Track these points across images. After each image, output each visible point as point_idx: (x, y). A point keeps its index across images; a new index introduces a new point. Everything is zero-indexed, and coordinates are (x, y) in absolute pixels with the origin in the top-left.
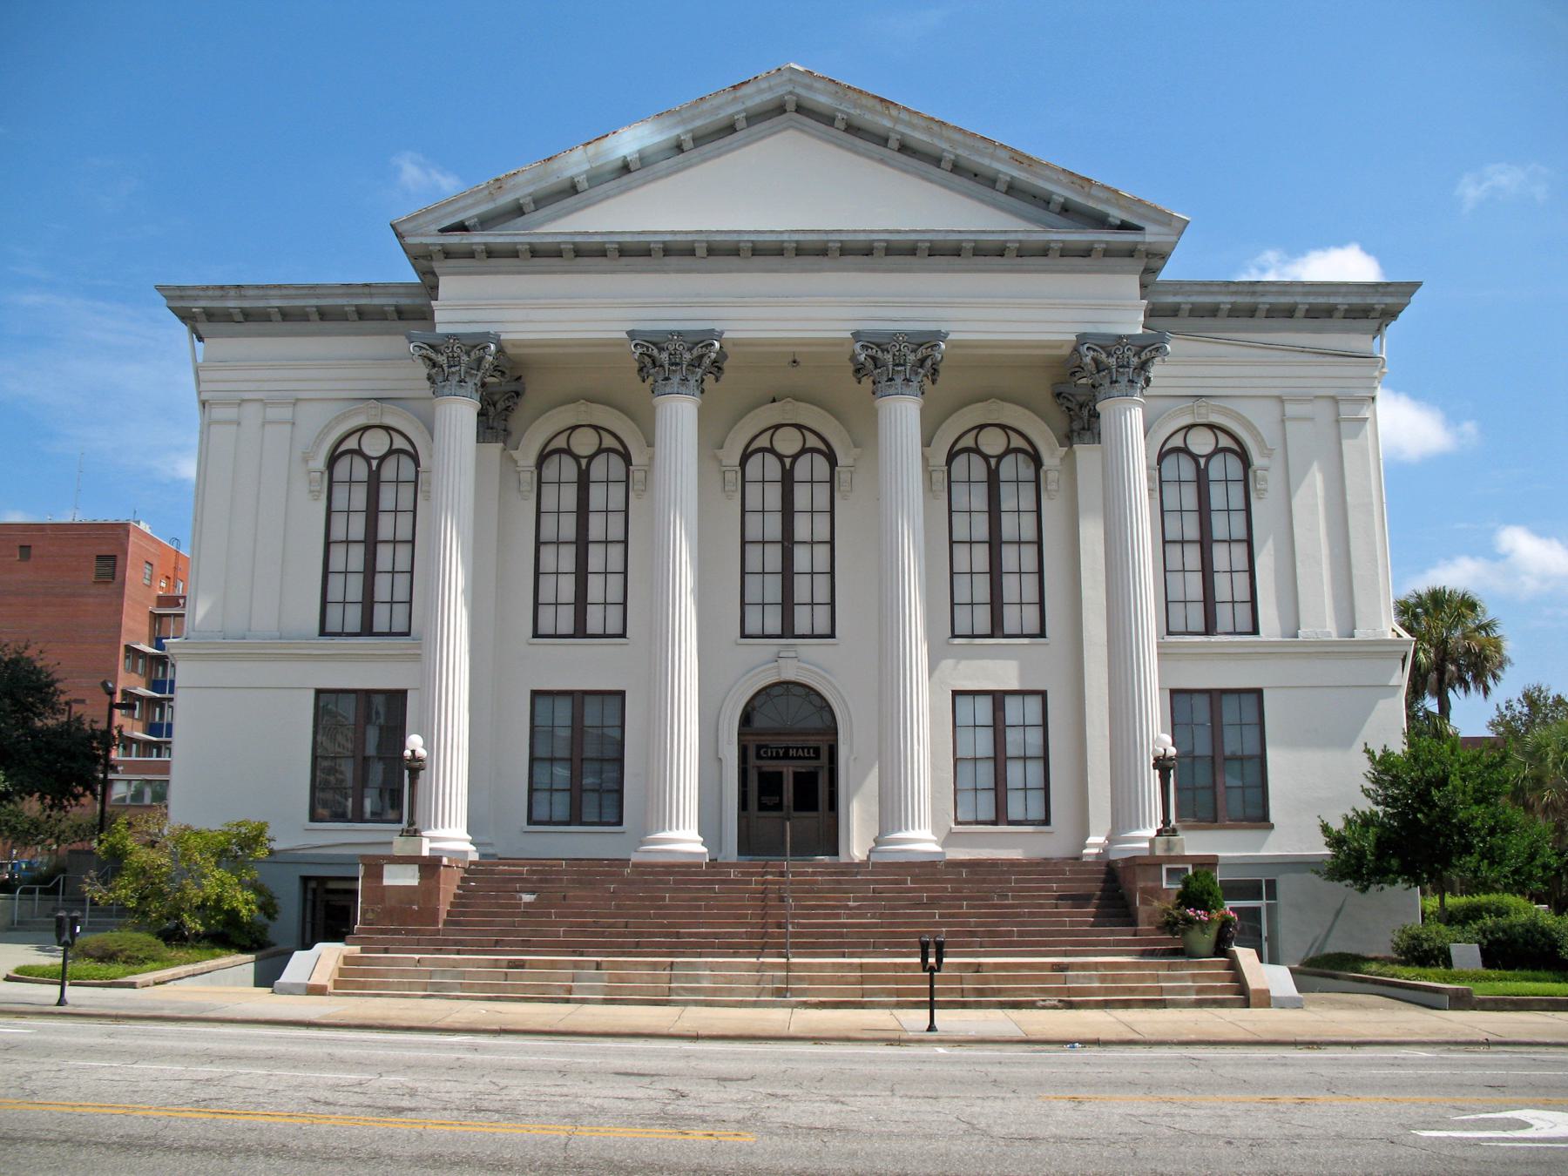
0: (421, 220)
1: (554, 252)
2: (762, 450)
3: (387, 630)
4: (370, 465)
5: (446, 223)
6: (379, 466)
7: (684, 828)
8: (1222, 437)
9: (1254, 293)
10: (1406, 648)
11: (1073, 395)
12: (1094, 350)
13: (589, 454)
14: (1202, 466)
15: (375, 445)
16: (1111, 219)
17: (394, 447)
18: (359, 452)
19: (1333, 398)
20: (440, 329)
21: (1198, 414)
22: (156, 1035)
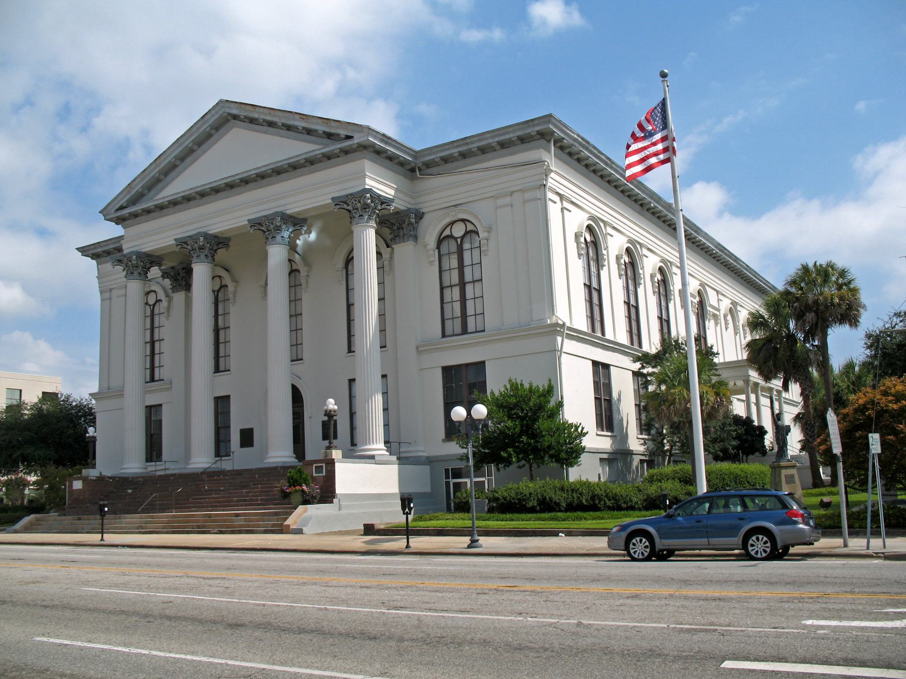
0: (109, 209)
1: (161, 208)
2: (447, 237)
5: (117, 207)
9: (467, 144)
11: (388, 221)
12: (338, 205)
15: (458, 231)
20: (125, 252)
22: (33, 551)
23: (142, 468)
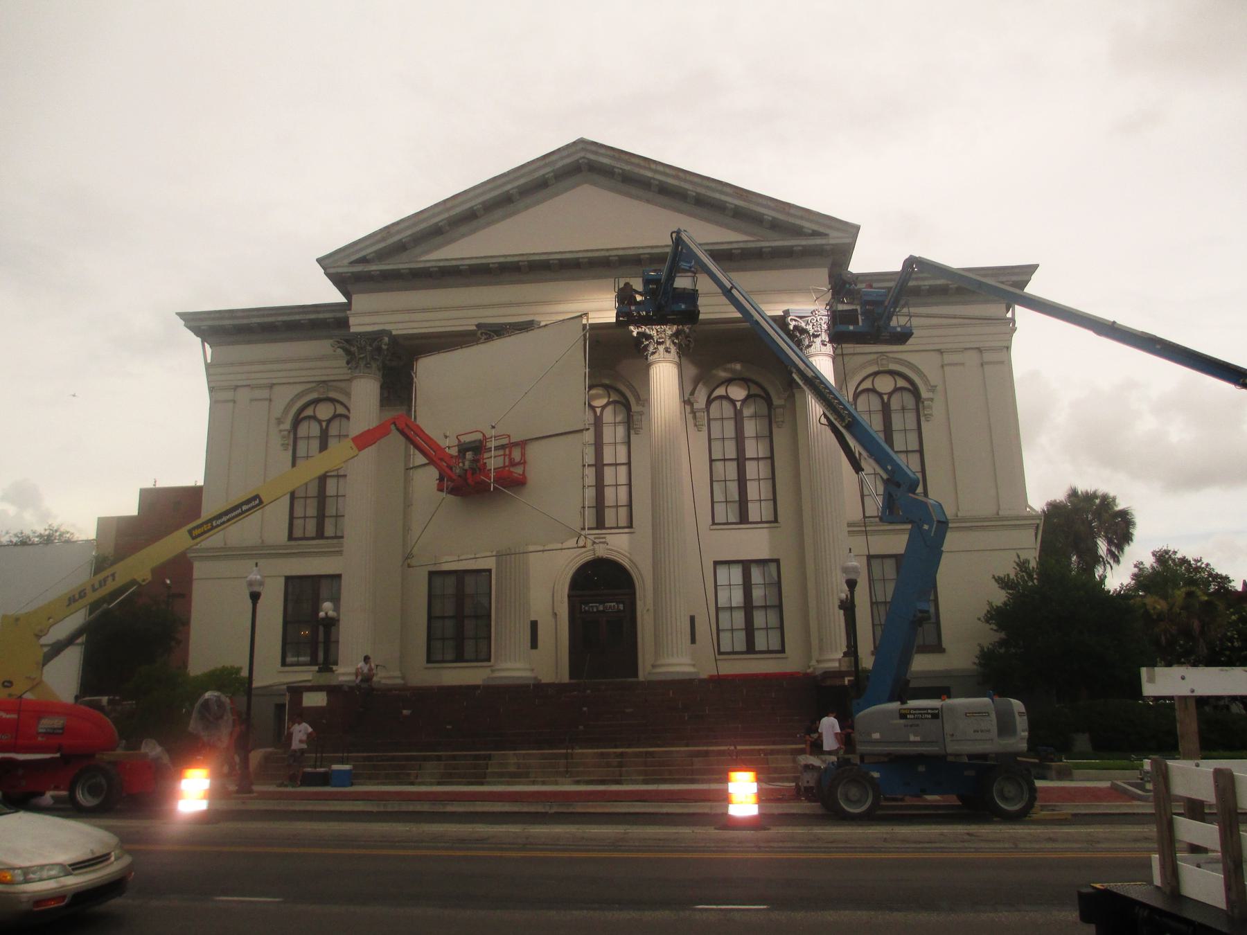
2: (309, 417)
3: (759, 520)
4: (321, 426)
6: (327, 426)
7: (678, 656)
8: (338, 406)
10: (1038, 521)
12: (795, 320)
13: (327, 418)
14: (598, 414)
16: (806, 230)
17: (337, 413)
18: (314, 418)
19: (978, 349)
20: (353, 330)
21: (882, 365)
23: (689, 665)
